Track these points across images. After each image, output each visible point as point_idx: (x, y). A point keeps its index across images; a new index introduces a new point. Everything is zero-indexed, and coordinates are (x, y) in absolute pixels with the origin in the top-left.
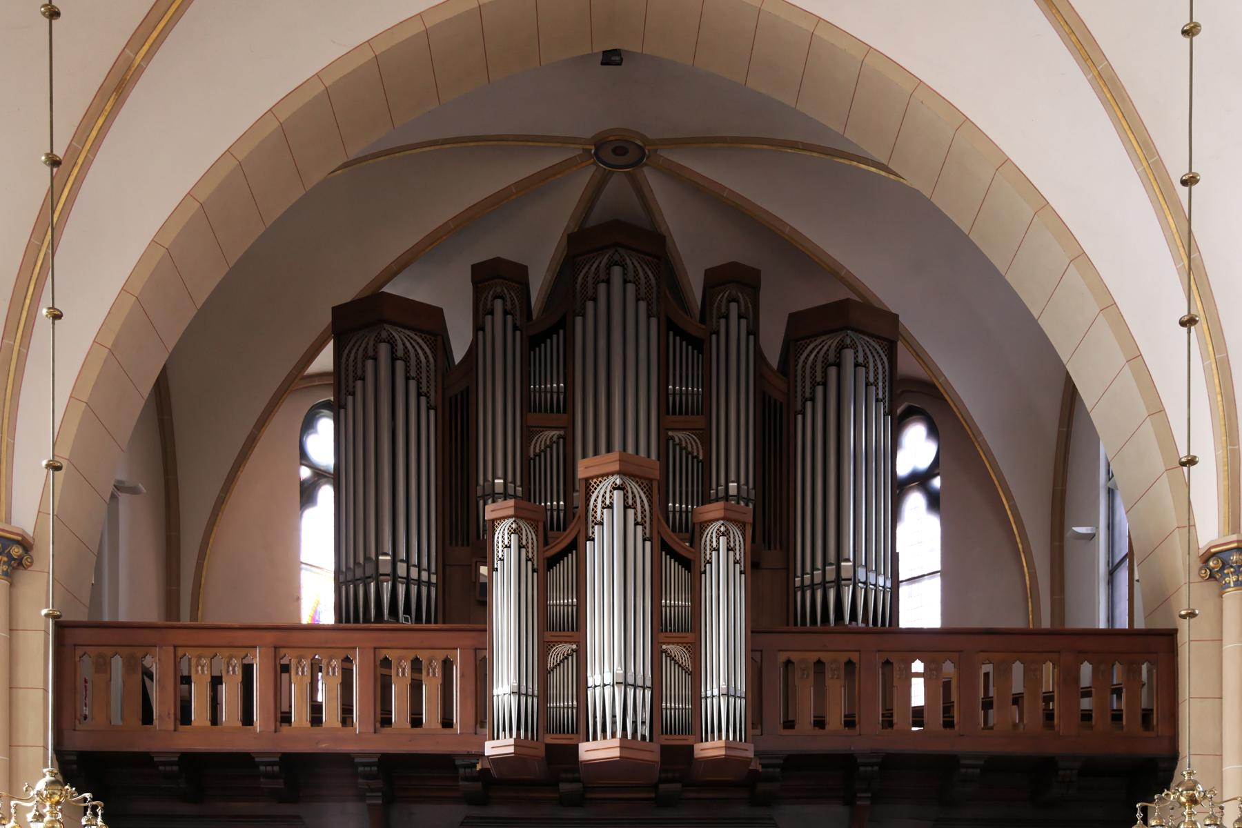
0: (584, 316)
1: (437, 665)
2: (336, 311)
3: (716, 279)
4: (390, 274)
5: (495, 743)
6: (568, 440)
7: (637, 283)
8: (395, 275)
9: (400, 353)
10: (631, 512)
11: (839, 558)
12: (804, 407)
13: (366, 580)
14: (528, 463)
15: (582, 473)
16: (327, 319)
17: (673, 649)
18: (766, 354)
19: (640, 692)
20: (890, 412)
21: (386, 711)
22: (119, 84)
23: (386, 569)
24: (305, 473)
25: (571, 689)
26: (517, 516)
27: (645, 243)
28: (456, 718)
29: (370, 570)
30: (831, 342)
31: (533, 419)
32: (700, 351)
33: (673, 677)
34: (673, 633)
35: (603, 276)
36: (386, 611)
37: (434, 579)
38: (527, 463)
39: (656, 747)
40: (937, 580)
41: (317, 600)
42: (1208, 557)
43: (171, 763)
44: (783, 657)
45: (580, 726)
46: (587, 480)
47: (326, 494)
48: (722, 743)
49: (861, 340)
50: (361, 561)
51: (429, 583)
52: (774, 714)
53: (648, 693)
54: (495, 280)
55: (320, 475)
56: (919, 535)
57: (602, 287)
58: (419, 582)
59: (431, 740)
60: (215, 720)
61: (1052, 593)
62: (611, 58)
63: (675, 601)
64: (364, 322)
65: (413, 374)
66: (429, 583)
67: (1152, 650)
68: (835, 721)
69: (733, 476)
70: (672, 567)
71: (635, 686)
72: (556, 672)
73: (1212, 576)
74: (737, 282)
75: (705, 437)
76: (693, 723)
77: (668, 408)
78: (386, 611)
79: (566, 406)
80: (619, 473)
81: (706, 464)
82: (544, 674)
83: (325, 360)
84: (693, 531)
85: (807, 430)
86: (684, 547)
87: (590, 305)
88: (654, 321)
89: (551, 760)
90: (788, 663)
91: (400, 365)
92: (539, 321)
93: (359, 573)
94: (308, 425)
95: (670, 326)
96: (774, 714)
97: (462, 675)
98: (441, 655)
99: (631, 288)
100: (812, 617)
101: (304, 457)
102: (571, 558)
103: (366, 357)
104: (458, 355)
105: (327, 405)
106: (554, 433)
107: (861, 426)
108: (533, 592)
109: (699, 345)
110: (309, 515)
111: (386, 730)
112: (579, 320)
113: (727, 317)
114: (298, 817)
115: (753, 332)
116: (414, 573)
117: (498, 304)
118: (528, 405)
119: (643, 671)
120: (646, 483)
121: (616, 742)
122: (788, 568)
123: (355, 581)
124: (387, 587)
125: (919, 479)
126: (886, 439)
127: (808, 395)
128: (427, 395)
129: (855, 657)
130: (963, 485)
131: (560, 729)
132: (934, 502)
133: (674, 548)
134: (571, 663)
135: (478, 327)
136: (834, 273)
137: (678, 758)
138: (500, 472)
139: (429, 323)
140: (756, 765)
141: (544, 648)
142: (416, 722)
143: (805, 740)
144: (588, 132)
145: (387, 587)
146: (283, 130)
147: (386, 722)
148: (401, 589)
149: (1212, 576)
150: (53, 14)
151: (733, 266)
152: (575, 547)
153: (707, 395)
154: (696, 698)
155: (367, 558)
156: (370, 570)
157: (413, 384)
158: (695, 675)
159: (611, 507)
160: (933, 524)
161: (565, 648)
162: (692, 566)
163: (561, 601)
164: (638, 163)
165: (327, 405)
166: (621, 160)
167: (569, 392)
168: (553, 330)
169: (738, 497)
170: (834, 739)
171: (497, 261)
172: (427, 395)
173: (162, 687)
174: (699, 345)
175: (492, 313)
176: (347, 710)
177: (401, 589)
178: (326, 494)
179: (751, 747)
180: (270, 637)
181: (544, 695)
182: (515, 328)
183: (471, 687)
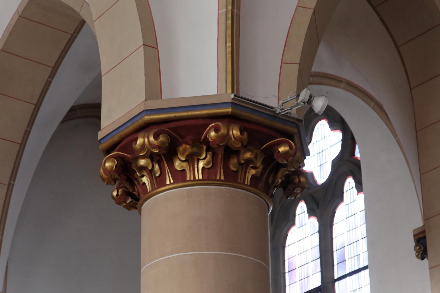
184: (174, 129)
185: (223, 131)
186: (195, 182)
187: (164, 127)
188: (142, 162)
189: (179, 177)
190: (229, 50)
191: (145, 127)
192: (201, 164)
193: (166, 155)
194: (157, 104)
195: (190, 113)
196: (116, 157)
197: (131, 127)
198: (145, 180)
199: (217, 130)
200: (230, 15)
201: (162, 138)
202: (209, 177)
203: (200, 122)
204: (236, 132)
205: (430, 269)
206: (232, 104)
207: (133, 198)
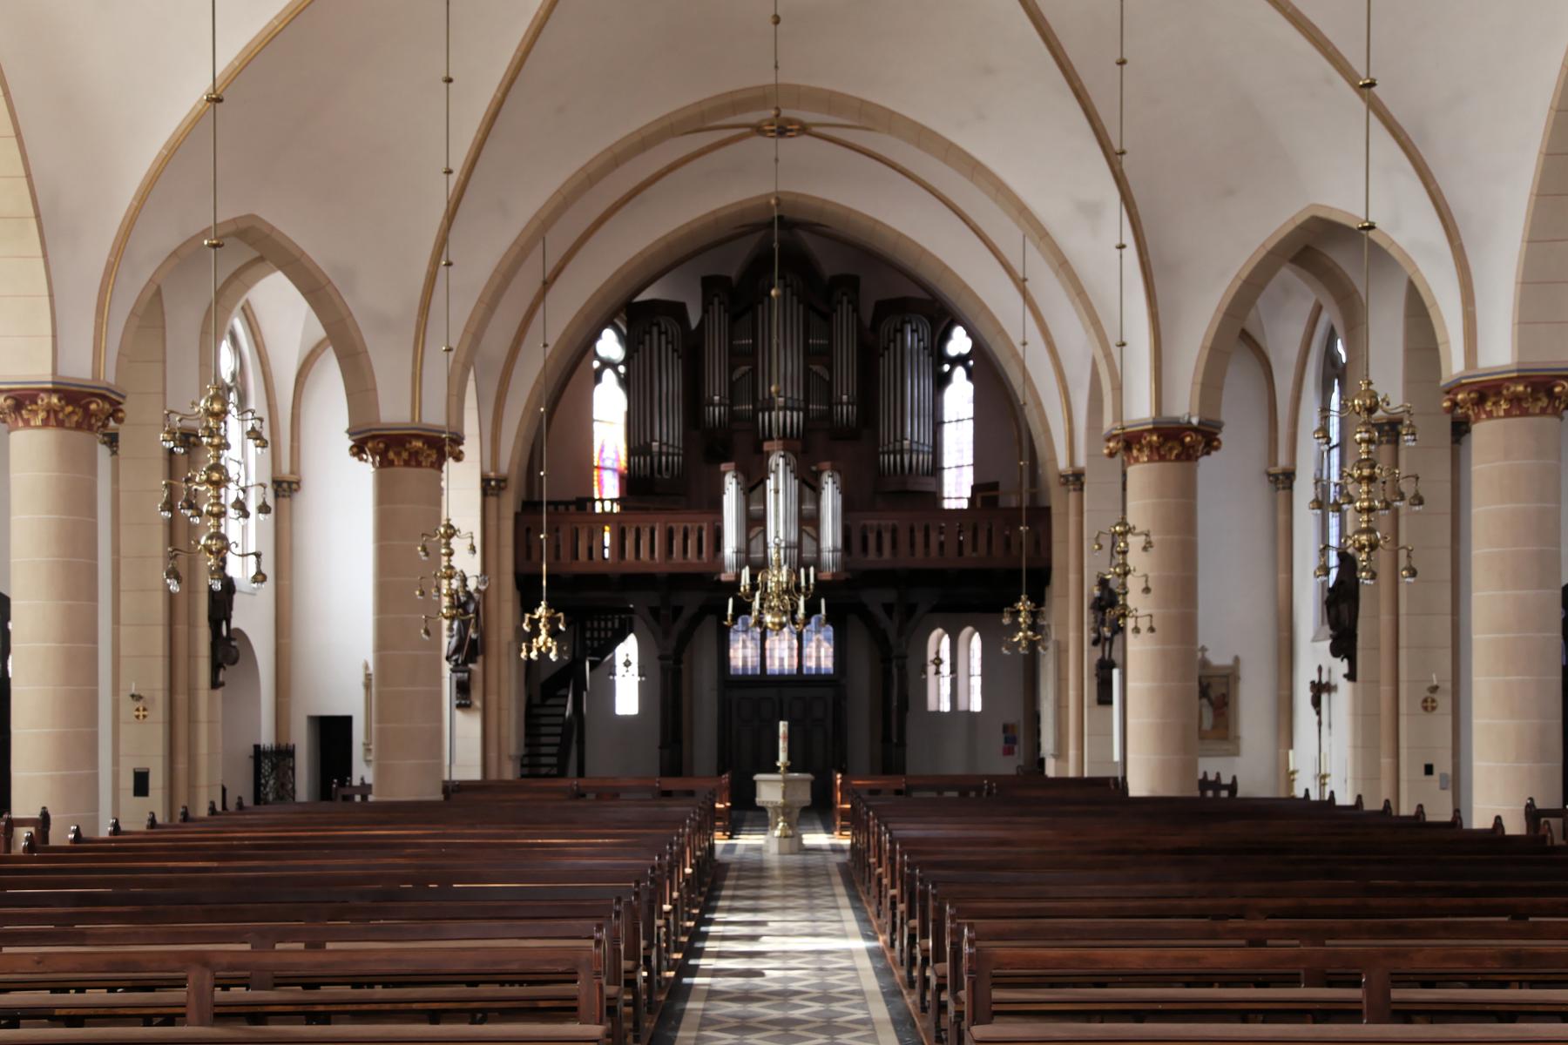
6: (754, 371)
14: (732, 386)
24: (596, 364)
25: (761, 548)
27: (798, 265)
54: (711, 286)
63: (808, 507)
70: (807, 491)
74: (850, 283)
75: (830, 369)
77: (810, 354)
82: (748, 541)
84: (817, 476)
85: (885, 365)
90: (864, 526)
98: (697, 526)
104: (694, 322)
108: (743, 504)
115: (856, 310)
119: (794, 537)
125: (960, 360)
132: (970, 376)
133: (809, 485)
134: (761, 537)
135: (705, 311)
150: (449, 80)
152: (762, 482)
154: (819, 551)
158: (817, 539)
160: (969, 388)
161: (745, 368)
162: (817, 491)
169: (848, 403)
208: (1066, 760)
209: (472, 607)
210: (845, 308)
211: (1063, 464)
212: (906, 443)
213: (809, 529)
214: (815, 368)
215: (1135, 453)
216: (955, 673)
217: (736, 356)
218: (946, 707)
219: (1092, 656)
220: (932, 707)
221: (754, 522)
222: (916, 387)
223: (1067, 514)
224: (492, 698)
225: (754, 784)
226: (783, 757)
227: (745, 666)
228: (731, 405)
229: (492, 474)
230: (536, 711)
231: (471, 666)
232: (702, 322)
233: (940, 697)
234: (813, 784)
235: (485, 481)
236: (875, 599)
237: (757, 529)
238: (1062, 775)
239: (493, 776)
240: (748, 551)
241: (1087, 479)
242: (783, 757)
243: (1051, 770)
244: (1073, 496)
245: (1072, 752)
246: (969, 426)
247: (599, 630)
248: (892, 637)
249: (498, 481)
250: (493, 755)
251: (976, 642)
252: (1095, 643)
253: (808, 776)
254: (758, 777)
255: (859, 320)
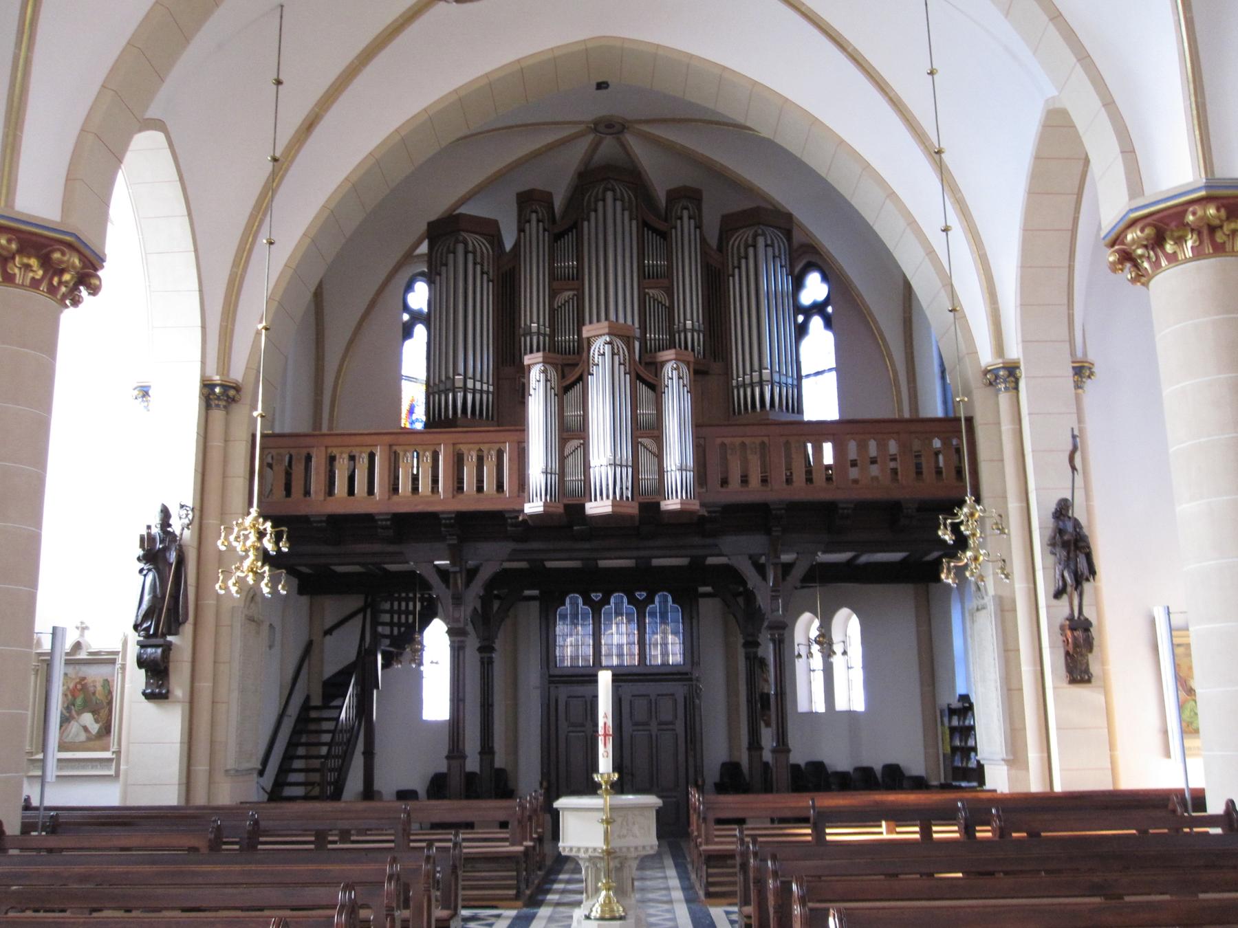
0: (589, 221)
1: (493, 453)
2: (429, 224)
3: (675, 195)
4: (463, 201)
5: (531, 504)
6: (580, 298)
7: (622, 200)
8: (468, 199)
9: (470, 248)
10: (616, 358)
11: (761, 368)
12: (739, 263)
13: (446, 392)
15: (585, 334)
16: (424, 227)
17: (646, 441)
18: (708, 240)
19: (624, 470)
20: (790, 273)
21: (461, 481)
22: (309, 126)
23: (459, 384)
24: (406, 317)
25: (580, 468)
26: (545, 362)
27: (627, 177)
28: (506, 487)
29: (449, 385)
30: (750, 233)
31: (556, 285)
32: (665, 239)
33: (645, 459)
34: (644, 432)
35: (600, 196)
36: (459, 411)
37: (491, 388)
38: (553, 312)
39: (636, 505)
40: (834, 374)
41: (413, 396)
42: (986, 372)
43: (321, 522)
44: (719, 441)
45: (586, 492)
46: (588, 339)
47: (420, 331)
48: (679, 501)
49: (769, 231)
50: (443, 378)
51: (488, 392)
52: (714, 477)
53: (630, 470)
54: (528, 201)
55: (417, 317)
56: (819, 347)
57: (600, 204)
58: (481, 391)
59: (489, 501)
60: (351, 492)
61: (909, 383)
62: (601, 86)
63: (646, 411)
64: (446, 233)
65: (479, 260)
66: (488, 392)
67: (957, 430)
68: (755, 481)
69: (688, 316)
70: (643, 390)
71: (621, 466)
72: (570, 459)
73: (991, 384)
74: (688, 197)
75: (670, 292)
76: (660, 489)
77: (645, 275)
78: (459, 411)
79: (578, 276)
80: (609, 334)
81: (670, 310)
82: (562, 459)
83: (424, 248)
84: (657, 367)
85: (735, 287)
86: (649, 377)
87: (593, 214)
88: (634, 223)
89: (568, 517)
90: (723, 445)
91: (470, 256)
92: (561, 221)
93: (442, 387)
94: (409, 287)
95: (645, 224)
96: (714, 477)
97: (510, 459)
99: (619, 203)
100: (738, 411)
101: (406, 308)
102: (579, 386)
103: (449, 252)
104: (508, 246)
105: (422, 274)
106: (571, 293)
107: (774, 280)
108: (555, 408)
109: (664, 235)
110: (408, 343)
111: (461, 496)
112: (586, 223)
113: (681, 218)
114: (401, 553)
115: (699, 227)
116: (478, 386)
117: (534, 216)
118: (553, 277)
119: (626, 453)
120: (628, 340)
121: (609, 502)
122: (727, 373)
123: (439, 393)
124: (460, 396)
125: (818, 308)
126: (788, 285)
127: (743, 254)
128: (487, 273)
129: (766, 439)
130: (844, 312)
131: (573, 494)
132: (828, 323)
133: (644, 376)
134: (580, 452)
135: (521, 230)
136: (747, 189)
137: (650, 509)
138: (535, 319)
139: (490, 230)
140: (704, 512)
141: (563, 441)
142: (480, 489)
143: (735, 493)
144: (589, 117)
145: (460, 396)
146: (403, 140)
147: (460, 488)
148: (470, 397)
149: (991, 384)
150: (279, 82)
151: (685, 188)
152: (581, 379)
153: (670, 267)
154: (661, 471)
155: (447, 378)
156: (449, 385)
157: (478, 267)
158: (659, 456)
159: (604, 354)
161: (568, 294)
162: (656, 388)
163: (572, 413)
164: (621, 132)
165: (422, 274)
166: (611, 131)
167: (580, 268)
168: (570, 229)
170: (754, 492)
171: (532, 191)
172: (487, 273)
173: (317, 474)
174: (664, 235)
175: (529, 221)
176: (435, 481)
177: (470, 397)
178: (420, 331)
179: (697, 502)
180: (387, 439)
181: (562, 473)
182: (545, 230)
183: (515, 467)
184: (1161, 220)
185: (1200, 213)
186: (1187, 260)
187: (1149, 220)
188: (1140, 251)
189: (1172, 258)
190: (1198, 137)
191: (1133, 223)
192: (1190, 243)
193: (1158, 242)
194: (1140, 202)
195: (586, 237)
196: (1116, 251)
197: (1122, 225)
198: (1146, 265)
199: (1194, 214)
200: (1194, 106)
201: (1147, 231)
202: (1198, 254)
203: (1180, 209)
204: (1212, 211)
205: (1007, 15)
206: (1207, 187)
207: (1141, 277)
208: (1025, 766)
209: (173, 557)
210: (687, 224)
211: (987, 357)
212: (766, 372)
213: (646, 441)
214: (651, 292)
215: (1169, 247)
216: (835, 669)
217: (557, 282)
218: (819, 706)
219: (1052, 613)
220: (802, 707)
221: (569, 434)
222: (774, 330)
223: (998, 424)
224: (205, 685)
225: (555, 815)
226: (605, 763)
227: (575, 658)
228: (552, 335)
229: (217, 378)
230: (313, 714)
231: (169, 638)
232: (517, 245)
233: (810, 695)
234: (659, 812)
235: (207, 387)
236: (735, 551)
237: (575, 443)
238: (1020, 789)
239: (200, 799)
240: (562, 473)
241: (1023, 373)
242: (605, 763)
243: (998, 780)
244: (1004, 399)
245: (1033, 755)
246: (831, 379)
247: (400, 612)
248: (763, 600)
249: (225, 387)
250: (201, 768)
251: (854, 624)
252: (1058, 594)
253: (653, 800)
254: (562, 803)
255: (703, 240)
